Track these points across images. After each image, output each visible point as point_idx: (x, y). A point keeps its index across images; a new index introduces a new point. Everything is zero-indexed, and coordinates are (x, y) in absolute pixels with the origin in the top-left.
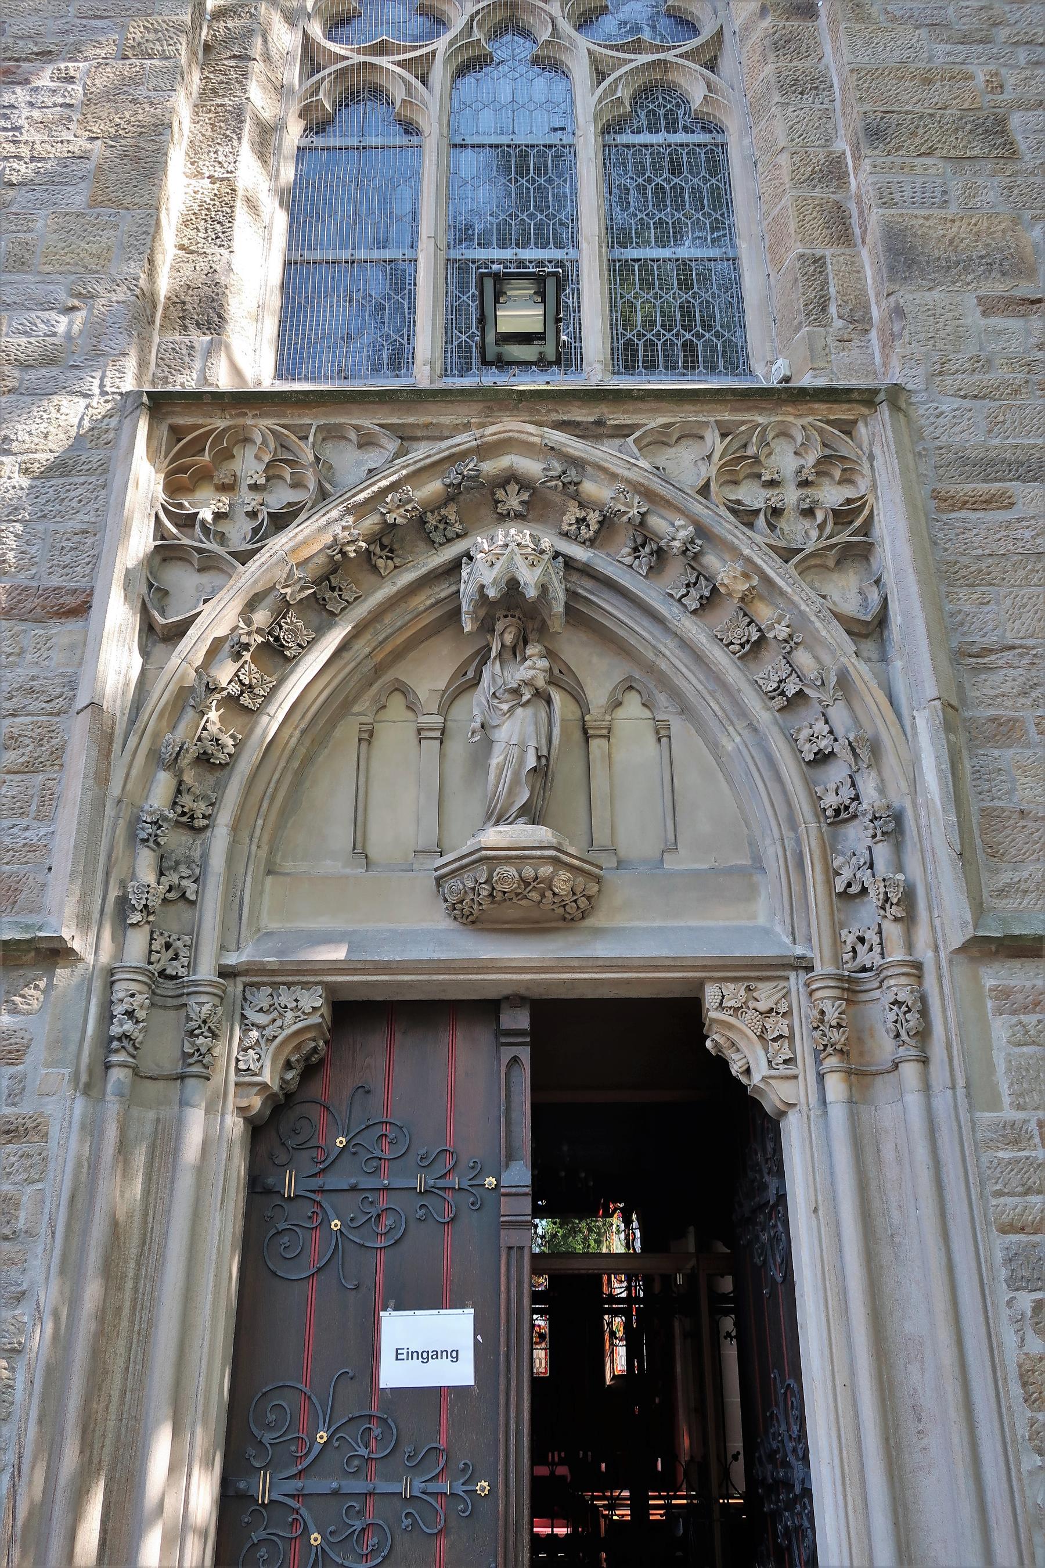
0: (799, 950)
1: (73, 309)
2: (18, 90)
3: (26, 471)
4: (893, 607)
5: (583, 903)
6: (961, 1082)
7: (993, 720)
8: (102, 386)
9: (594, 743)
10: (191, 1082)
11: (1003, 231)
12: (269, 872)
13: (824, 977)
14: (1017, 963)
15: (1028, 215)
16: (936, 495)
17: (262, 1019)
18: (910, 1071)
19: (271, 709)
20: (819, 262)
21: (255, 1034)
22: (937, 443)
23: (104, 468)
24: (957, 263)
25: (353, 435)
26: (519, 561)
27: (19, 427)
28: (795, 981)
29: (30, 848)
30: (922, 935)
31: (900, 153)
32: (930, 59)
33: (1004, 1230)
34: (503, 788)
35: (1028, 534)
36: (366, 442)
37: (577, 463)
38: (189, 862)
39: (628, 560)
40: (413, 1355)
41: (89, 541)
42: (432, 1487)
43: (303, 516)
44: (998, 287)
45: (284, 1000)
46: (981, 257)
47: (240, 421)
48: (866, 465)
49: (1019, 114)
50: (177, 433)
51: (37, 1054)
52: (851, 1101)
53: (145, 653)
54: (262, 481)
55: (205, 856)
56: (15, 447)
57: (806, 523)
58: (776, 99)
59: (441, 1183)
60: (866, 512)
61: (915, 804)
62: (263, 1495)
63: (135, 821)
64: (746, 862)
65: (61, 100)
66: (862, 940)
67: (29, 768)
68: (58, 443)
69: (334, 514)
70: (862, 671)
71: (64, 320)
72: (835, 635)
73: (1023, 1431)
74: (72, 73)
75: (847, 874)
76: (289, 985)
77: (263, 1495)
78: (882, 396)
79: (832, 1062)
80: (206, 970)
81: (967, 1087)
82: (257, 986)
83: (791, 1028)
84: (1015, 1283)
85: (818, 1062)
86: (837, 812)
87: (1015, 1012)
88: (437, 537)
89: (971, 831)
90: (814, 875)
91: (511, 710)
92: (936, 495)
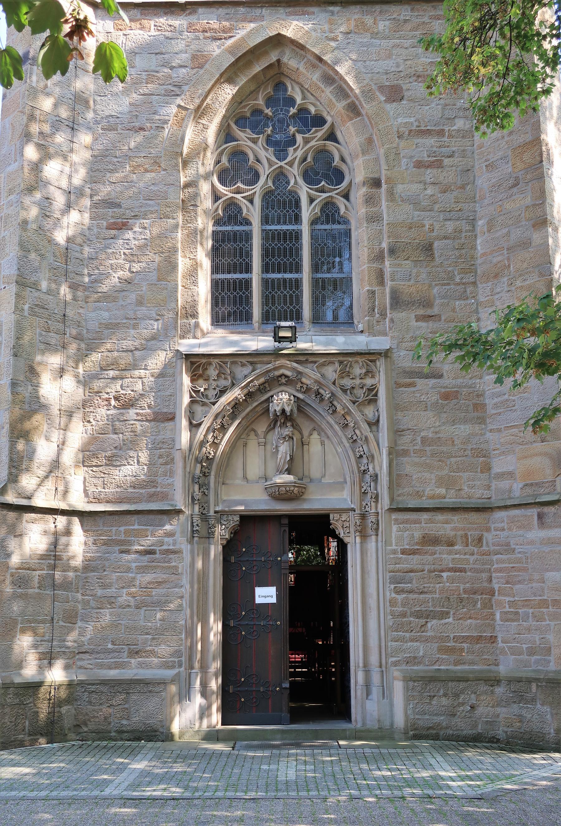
0: (352, 506)
1: (158, 320)
2: (129, 232)
3: (152, 376)
4: (381, 418)
5: (301, 494)
6: (384, 540)
7: (403, 450)
8: (170, 347)
9: (305, 446)
10: (211, 539)
11: (426, 290)
12: (223, 484)
13: (357, 514)
14: (400, 513)
15: (434, 283)
16: (396, 383)
17: (225, 523)
18: (374, 538)
19: (222, 443)
20: (373, 292)
21: (224, 526)
22: (398, 366)
23: (173, 375)
24: (411, 302)
25: (240, 363)
26: (285, 404)
27: (149, 361)
28: (351, 513)
29: (169, 485)
30: (379, 506)
31: (399, 259)
32: (412, 218)
33: (389, 572)
34: (281, 464)
35: (418, 395)
36: (243, 365)
37: (300, 373)
38: (205, 485)
39: (314, 398)
40: (264, 596)
41: (173, 398)
42: (268, 623)
43: (228, 391)
44: (421, 312)
45: (230, 518)
46: (418, 300)
47: (209, 360)
48: (378, 374)
49: (437, 242)
50: (192, 363)
51: (178, 535)
52: (361, 543)
53: (190, 431)
54: (216, 378)
55: (209, 483)
56: (149, 368)
57: (361, 390)
58: (365, 225)
59: (268, 559)
60: (376, 389)
61: (381, 473)
62: (232, 625)
63: (193, 478)
64: (342, 480)
65: (143, 237)
66: (367, 504)
67: (166, 464)
68: (160, 365)
69: (236, 390)
70: (371, 436)
71: (156, 323)
72: (364, 426)
73: (389, 611)
74: (146, 225)
75: (365, 488)
76: (231, 515)
77: (232, 625)
78: (383, 355)
79: (358, 534)
80: (212, 513)
81: (385, 541)
82: (224, 515)
83: (349, 525)
84: (390, 583)
85: (355, 534)
86: (364, 471)
87: (398, 524)
88: (263, 391)
89: (393, 482)
90: (357, 488)
91: (283, 442)
92: (396, 383)
